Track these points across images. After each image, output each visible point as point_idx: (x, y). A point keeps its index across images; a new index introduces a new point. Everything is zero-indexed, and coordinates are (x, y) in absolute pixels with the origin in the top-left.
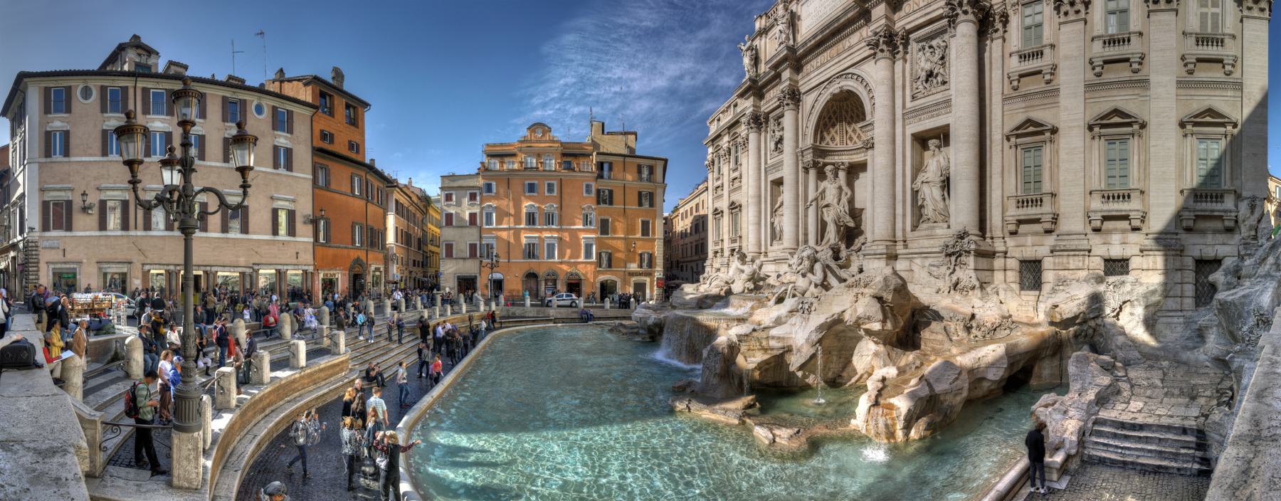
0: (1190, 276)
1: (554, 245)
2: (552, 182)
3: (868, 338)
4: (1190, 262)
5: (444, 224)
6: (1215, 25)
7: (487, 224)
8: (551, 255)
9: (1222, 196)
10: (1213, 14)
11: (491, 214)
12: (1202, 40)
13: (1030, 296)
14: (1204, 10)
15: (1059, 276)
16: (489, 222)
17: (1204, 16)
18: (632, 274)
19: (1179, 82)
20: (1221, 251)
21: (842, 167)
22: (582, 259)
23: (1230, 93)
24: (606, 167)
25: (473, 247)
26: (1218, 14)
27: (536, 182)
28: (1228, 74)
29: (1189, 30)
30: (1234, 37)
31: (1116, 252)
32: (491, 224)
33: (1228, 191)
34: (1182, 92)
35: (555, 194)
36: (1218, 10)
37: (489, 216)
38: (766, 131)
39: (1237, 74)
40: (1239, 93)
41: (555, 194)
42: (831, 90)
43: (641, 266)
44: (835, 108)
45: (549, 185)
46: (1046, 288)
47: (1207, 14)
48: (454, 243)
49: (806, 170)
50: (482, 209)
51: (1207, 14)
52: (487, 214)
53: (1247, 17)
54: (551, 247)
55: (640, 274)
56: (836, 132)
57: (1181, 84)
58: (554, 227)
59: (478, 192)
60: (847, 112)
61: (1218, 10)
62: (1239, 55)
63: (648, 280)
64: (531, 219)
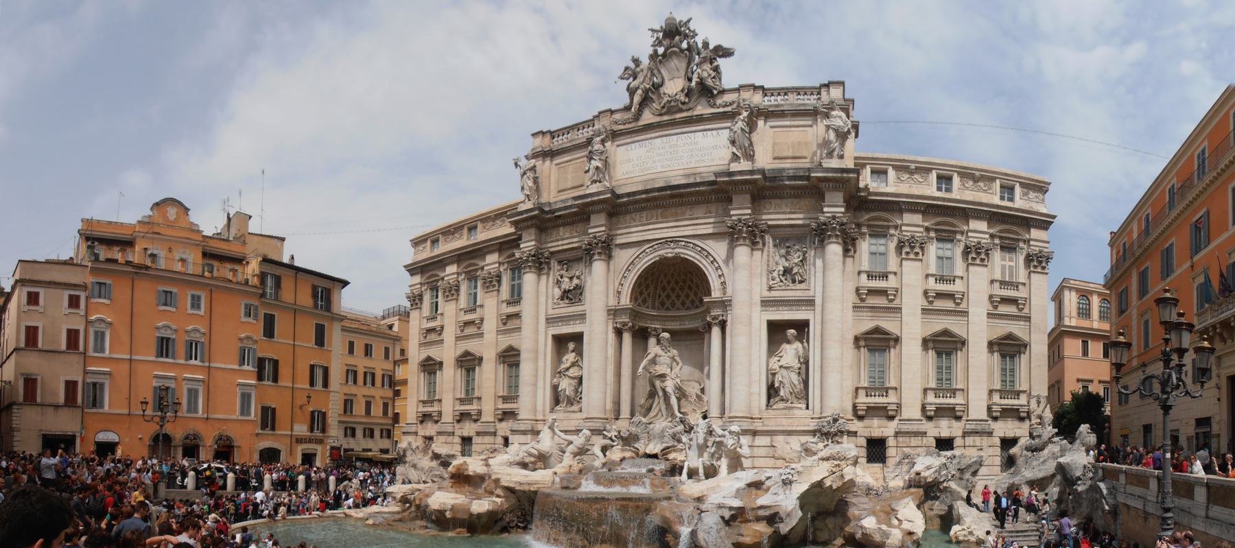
0: (998, 451)
1: (196, 391)
2: (198, 293)
3: (993, 515)
4: (998, 442)
5: (64, 347)
6: (1011, 275)
7: (96, 351)
8: (193, 407)
9: (1018, 395)
10: (1009, 266)
11: (103, 334)
12: (1003, 283)
13: (877, 467)
14: (1003, 263)
15: (904, 452)
16: (100, 347)
17: (1003, 267)
18: (300, 440)
19: (988, 314)
20: (1018, 433)
21: (654, 333)
22: (237, 415)
23: (1022, 323)
24: (270, 282)
25: (71, 386)
26: (1012, 266)
27: (174, 290)
28: (958, 304)
29: (863, 268)
30: (895, 274)
31: (945, 434)
32: (102, 350)
33: (1024, 392)
34: (991, 320)
35: (202, 312)
36: (1013, 264)
37: (100, 336)
38: (548, 275)
39: (1026, 310)
40: (1028, 323)
41: (202, 312)
42: (661, 252)
43: (312, 430)
44: (655, 270)
45: (193, 297)
46: (891, 462)
47: (1005, 266)
48: (39, 378)
49: (619, 333)
50: (88, 322)
51: (1005, 266)
52: (96, 332)
53: (1034, 272)
54: (193, 394)
55: (310, 441)
56: (649, 295)
57: (990, 315)
58: (197, 363)
59: (83, 295)
60: (666, 275)
61: (1013, 264)
62: (966, 291)
63: (319, 448)
64: (164, 347)
